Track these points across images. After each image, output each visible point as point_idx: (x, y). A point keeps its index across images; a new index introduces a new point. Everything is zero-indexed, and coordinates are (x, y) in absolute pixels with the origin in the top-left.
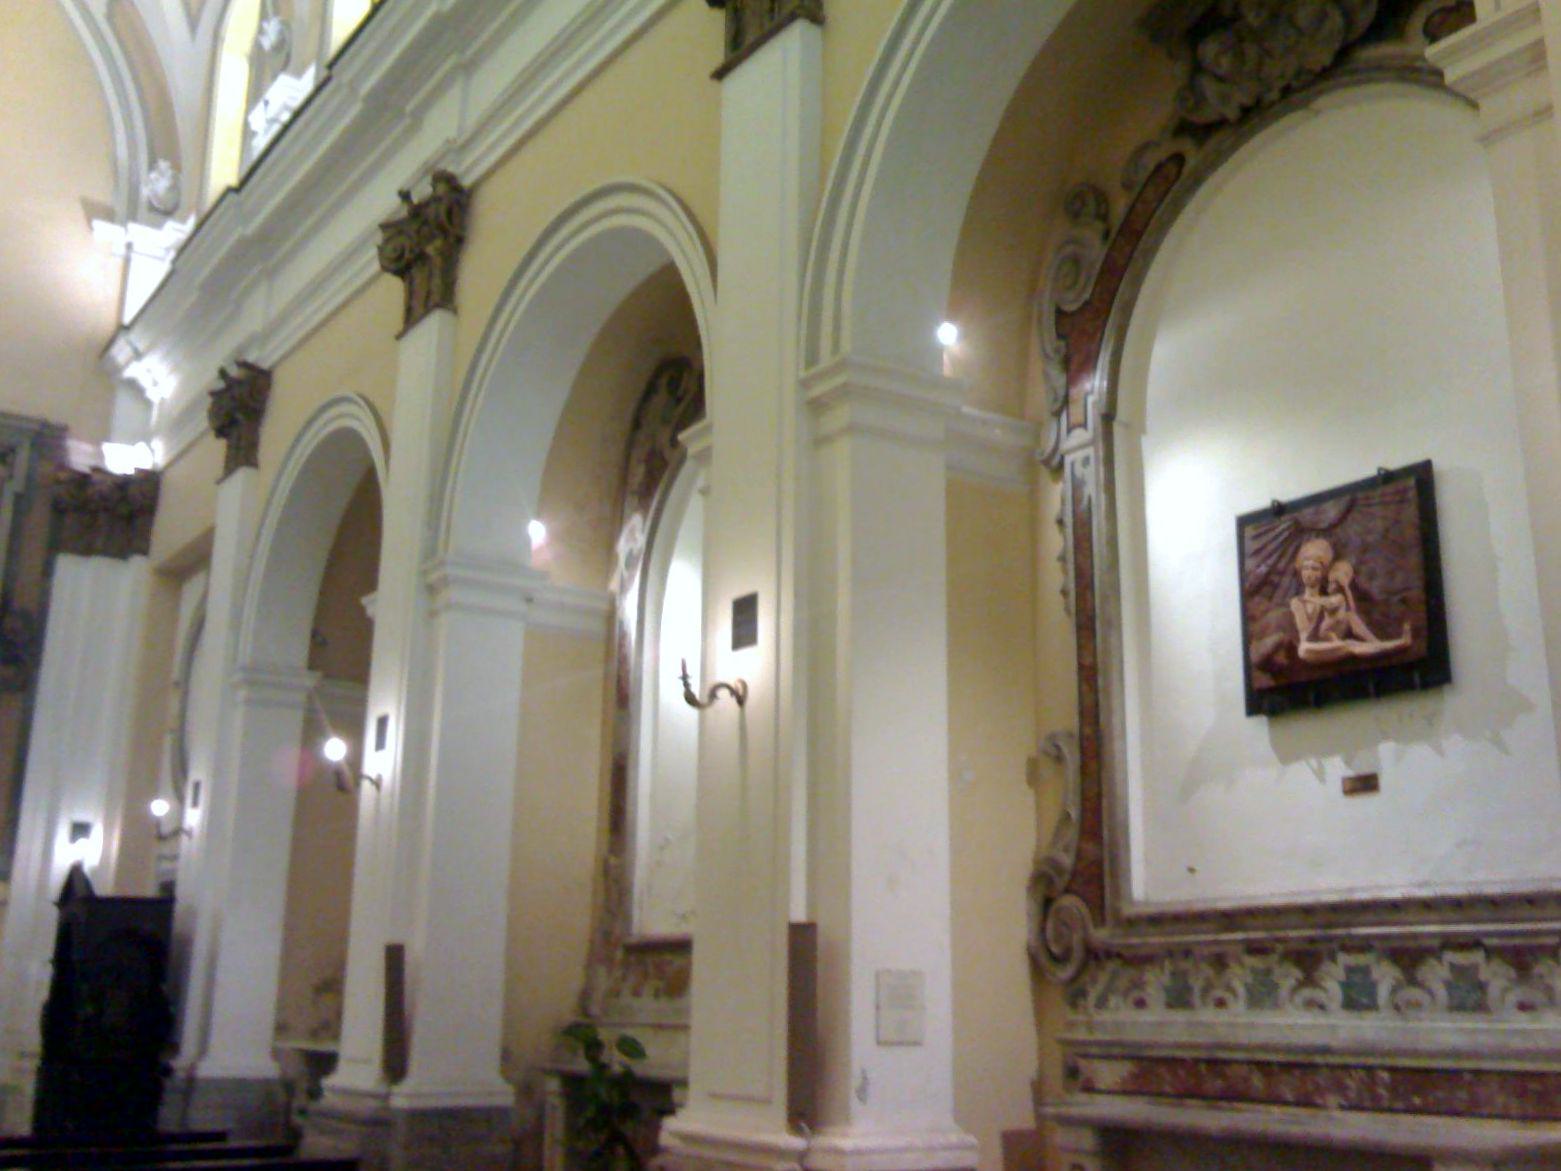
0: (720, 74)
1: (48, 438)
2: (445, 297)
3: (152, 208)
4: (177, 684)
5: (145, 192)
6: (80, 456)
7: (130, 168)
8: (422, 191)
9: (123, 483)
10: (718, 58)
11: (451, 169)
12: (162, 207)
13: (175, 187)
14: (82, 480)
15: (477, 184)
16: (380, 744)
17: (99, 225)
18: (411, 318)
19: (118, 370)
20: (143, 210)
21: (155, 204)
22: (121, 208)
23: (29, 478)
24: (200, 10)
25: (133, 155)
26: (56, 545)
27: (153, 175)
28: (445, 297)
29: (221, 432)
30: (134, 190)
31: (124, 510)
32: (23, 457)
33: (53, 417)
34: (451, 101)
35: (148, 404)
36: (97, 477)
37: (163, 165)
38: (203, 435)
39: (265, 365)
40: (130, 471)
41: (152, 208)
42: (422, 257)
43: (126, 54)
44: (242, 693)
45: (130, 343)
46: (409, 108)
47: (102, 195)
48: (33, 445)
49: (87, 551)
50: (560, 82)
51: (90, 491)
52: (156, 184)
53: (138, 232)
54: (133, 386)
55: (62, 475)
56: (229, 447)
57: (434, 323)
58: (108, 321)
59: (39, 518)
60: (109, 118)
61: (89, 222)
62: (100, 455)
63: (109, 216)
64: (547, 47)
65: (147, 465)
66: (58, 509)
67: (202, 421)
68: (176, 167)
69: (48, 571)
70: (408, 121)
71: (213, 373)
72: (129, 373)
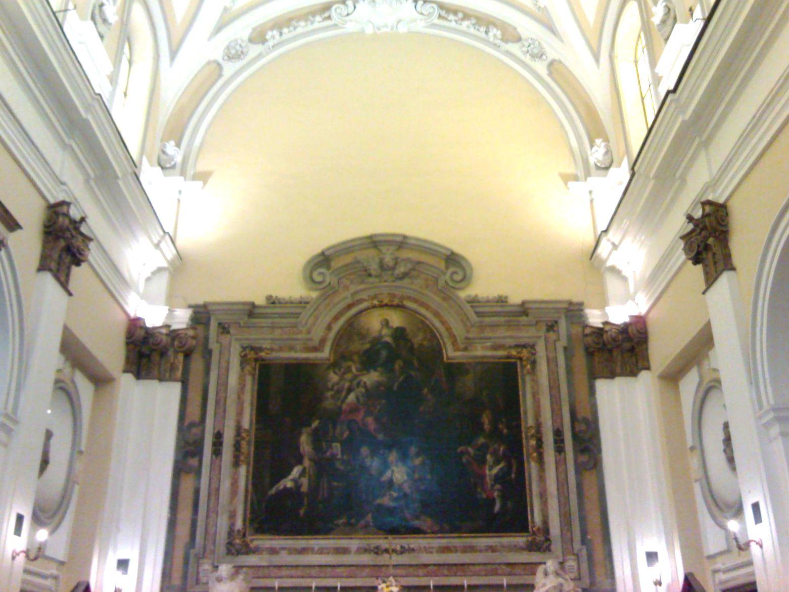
0: (704, 293)
1: (574, 311)
2: (728, 265)
3: (598, 168)
4: (692, 448)
5: (592, 160)
6: (594, 318)
7: (580, 151)
8: (698, 214)
9: (624, 329)
10: (704, 287)
11: (711, 197)
12: (603, 166)
13: (608, 152)
14: (599, 332)
15: (727, 200)
16: (758, 518)
17: (570, 184)
18: (710, 280)
19: (603, 262)
20: (593, 169)
21: (599, 164)
22: (581, 174)
23: (570, 337)
24: (599, 52)
25: (580, 143)
26: (593, 376)
27: (595, 148)
28: (728, 265)
29: (696, 260)
30: (586, 161)
31: (627, 345)
32: (563, 326)
33: (575, 299)
34: (702, 160)
35: (625, 279)
36: (607, 328)
37: (598, 141)
38: (683, 264)
39: (721, 201)
40: (627, 320)
41: (598, 168)
42: (707, 247)
43: (563, 90)
44: (775, 430)
45: (609, 240)
46: (678, 175)
47: (571, 170)
48: (566, 316)
49: (612, 375)
50: (760, 139)
51: (605, 336)
52: (597, 154)
53: (595, 181)
54: (614, 270)
55: (588, 331)
56: (703, 266)
57: (725, 279)
58: (590, 240)
59: (580, 360)
60: (562, 126)
61: (566, 184)
62: (606, 315)
63: (576, 178)
64: (665, 253)
65: (636, 313)
66: (590, 353)
67: (680, 256)
68: (607, 140)
69: (592, 391)
70: (678, 183)
71: (684, 219)
72: (609, 264)
